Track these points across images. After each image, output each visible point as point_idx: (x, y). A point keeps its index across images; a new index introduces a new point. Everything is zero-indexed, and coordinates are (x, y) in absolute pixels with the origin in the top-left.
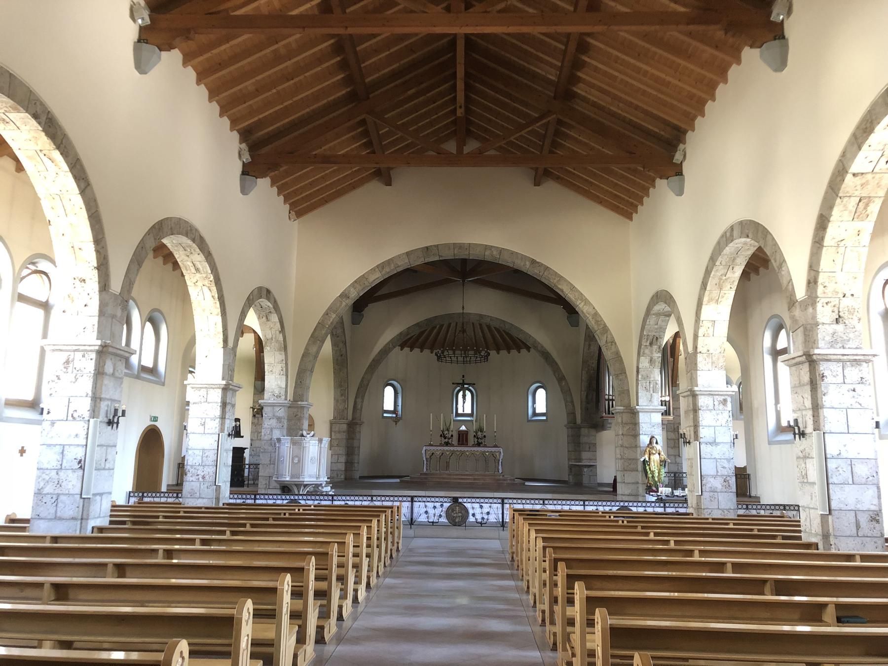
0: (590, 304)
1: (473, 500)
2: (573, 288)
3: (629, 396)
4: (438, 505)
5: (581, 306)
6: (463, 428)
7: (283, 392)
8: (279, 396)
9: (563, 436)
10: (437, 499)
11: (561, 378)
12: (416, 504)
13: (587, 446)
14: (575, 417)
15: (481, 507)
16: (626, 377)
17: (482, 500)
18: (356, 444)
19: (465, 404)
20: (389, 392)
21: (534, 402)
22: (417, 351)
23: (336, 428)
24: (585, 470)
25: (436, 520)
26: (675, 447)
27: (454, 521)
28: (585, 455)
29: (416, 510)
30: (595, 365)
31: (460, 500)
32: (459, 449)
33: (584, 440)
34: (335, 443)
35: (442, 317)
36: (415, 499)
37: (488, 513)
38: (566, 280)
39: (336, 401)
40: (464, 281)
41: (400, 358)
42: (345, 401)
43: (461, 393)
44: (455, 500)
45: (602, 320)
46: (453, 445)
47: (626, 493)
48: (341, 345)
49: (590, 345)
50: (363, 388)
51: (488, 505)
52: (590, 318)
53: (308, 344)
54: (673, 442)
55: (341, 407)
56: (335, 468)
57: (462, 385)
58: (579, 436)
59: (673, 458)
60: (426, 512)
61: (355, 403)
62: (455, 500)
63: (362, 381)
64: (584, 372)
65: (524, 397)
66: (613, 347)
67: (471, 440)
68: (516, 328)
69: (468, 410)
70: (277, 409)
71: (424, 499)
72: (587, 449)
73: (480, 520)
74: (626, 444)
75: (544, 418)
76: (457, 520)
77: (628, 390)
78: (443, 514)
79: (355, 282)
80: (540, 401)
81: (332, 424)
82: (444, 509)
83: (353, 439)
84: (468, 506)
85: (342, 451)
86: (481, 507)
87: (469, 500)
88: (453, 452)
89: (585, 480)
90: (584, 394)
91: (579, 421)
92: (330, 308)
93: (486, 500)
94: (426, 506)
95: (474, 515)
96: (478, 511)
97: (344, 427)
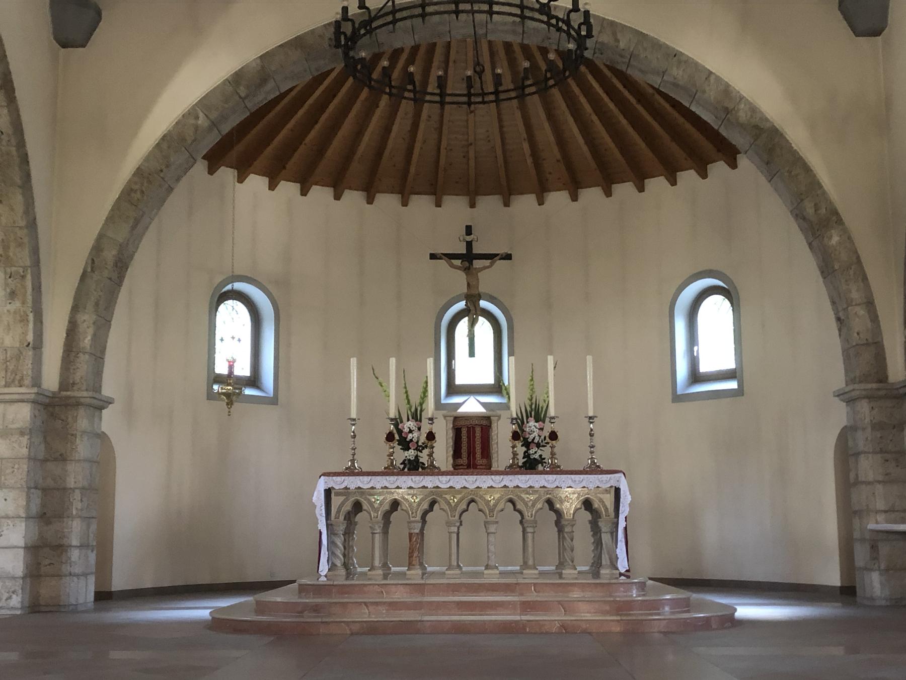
20: (232, 320)
22: (320, 194)
32: (460, 481)
41: (261, 210)
42: (24, 320)
43: (463, 325)
46: (432, 470)
50: (106, 274)
63: (97, 248)
67: (504, 448)
68: (657, 45)
75: (733, 385)
80: (715, 336)
83: (63, 459)
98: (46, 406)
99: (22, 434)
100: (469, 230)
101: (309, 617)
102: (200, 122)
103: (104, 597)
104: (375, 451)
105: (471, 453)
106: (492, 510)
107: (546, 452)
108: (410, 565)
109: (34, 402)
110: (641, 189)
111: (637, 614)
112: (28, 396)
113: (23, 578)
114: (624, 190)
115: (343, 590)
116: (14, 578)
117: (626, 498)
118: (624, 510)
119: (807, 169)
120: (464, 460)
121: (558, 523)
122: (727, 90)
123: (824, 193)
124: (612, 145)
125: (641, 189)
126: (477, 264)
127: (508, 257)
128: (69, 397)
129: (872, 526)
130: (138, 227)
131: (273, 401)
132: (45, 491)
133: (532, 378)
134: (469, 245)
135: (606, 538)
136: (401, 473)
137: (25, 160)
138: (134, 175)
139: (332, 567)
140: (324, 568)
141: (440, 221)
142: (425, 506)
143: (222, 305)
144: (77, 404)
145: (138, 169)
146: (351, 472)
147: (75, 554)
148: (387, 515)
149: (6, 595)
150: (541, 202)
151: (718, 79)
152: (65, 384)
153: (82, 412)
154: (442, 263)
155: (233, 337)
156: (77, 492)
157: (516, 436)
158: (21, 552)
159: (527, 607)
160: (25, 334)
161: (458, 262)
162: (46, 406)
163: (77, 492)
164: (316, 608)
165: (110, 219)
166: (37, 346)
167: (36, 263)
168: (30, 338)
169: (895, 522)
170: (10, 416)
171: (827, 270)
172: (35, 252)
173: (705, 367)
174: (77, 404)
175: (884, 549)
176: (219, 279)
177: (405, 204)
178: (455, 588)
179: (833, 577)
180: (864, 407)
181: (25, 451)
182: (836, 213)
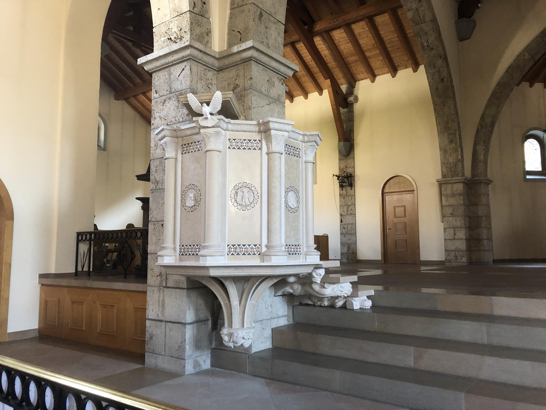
23: (448, 189)
34: (449, 211)
39: (444, 151)
42: (456, 151)
48: (439, 63)
56: (453, 248)
81: (441, 184)
83: (476, 205)
85: (459, 222)
97: (460, 187)
99: (460, 195)
102: (526, 57)
103: (494, 261)
109: (464, 183)
112: (461, 180)
113: (466, 251)
116: (462, 251)
128: (477, 180)
132: (470, 218)
138: (496, 86)
143: (526, 142)
144: (479, 182)
145: (498, 83)
149: (460, 258)
152: (473, 176)
153: (483, 186)
155: (532, 156)
156: (484, 217)
158: (464, 241)
160: (457, 156)
163: (484, 217)
165: (487, 107)
166: (462, 161)
167: (459, 127)
168: (460, 157)
172: (459, 123)
174: (479, 182)
176: (525, 130)
181: (462, 202)
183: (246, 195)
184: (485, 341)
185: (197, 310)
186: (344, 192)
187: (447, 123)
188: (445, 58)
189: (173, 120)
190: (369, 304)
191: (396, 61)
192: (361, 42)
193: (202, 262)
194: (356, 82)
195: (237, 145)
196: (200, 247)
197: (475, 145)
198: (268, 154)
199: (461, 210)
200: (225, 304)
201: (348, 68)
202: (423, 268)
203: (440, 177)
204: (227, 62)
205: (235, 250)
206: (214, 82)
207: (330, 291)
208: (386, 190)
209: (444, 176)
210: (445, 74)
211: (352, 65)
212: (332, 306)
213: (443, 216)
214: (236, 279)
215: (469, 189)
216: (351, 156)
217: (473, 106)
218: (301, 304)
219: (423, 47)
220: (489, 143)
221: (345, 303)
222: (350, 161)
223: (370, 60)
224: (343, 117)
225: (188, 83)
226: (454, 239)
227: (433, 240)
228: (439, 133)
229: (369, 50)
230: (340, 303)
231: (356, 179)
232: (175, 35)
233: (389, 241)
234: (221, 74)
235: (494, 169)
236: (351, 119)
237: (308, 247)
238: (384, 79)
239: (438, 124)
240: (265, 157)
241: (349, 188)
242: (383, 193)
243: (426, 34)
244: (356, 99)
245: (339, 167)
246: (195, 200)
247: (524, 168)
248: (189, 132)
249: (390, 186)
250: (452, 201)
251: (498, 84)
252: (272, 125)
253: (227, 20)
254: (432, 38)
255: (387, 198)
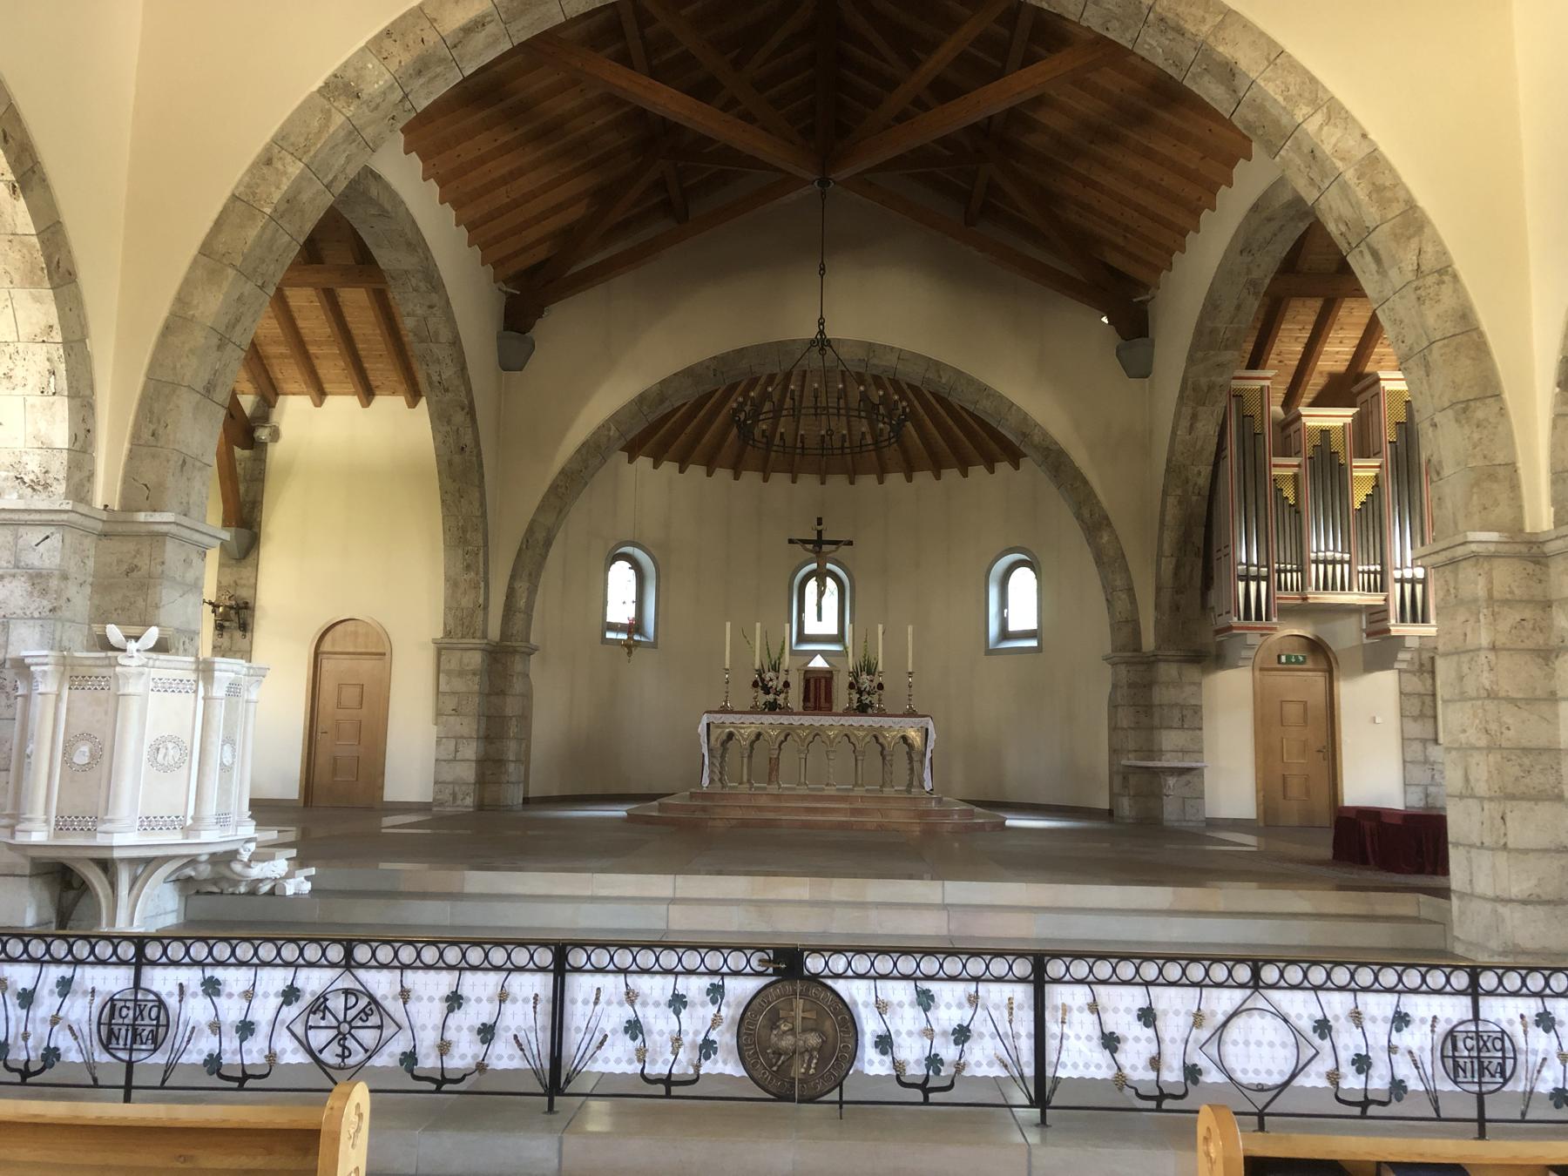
0: (1348, 119)
1: (884, 964)
2: (1276, 55)
3: (1515, 486)
4: (695, 987)
5: (1311, 127)
6: (819, 663)
7: (59, 466)
8: (39, 485)
9: (1094, 689)
10: (691, 959)
11: (1094, 523)
12: (580, 987)
13: (1176, 713)
14: (1136, 633)
15: (925, 1000)
16: (1502, 411)
17: (929, 965)
18: (511, 707)
19: (822, 612)
20: (621, 578)
21: (1003, 603)
22: (696, 471)
23: (452, 661)
24: (1171, 781)
25: (683, 1068)
26: (1422, 715)
27: (782, 1072)
28: (1170, 740)
29: (578, 1014)
30: (1203, 481)
31: (814, 964)
32: (807, 720)
33: (1162, 695)
34: (450, 703)
35: (760, 350)
36: (577, 957)
37: (962, 1034)
38: (1247, 26)
39: (452, 583)
40: (824, 182)
41: (649, 485)
42: (476, 587)
43: (812, 586)
44: (787, 962)
45: (1398, 183)
47: (1515, 891)
48: (459, 418)
49: (1194, 417)
50: (534, 550)
51: (961, 990)
52: (1350, 175)
53: (187, 282)
54: (1416, 701)
55: (466, 602)
56: (449, 778)
57: (819, 548)
58: (1148, 685)
59: (1417, 746)
60: (634, 1028)
61: (511, 594)
62: (787, 962)
63: (530, 530)
64: (1171, 501)
65: (978, 586)
66: (1447, 290)
67: (842, 696)
68: (971, 381)
69: (829, 626)
70: (33, 536)
71: (624, 958)
72: (1176, 723)
73: (916, 1070)
74: (1506, 687)
75: (1034, 643)
76: (798, 1070)
77: (1512, 466)
78: (725, 1038)
79: (388, 33)
80: (1023, 602)
81: (441, 649)
82: (730, 1012)
83: (502, 693)
84: (856, 992)
85: (467, 726)
86: (925, 1000)
87: (861, 964)
88: (788, 733)
89: (1171, 812)
90: (1168, 566)
91: (1149, 641)
92: (280, 140)
93: (953, 966)
94: (631, 997)
95: (884, 1043)
96: (906, 1021)
97: (475, 659)
98: (491, 652)
99: (474, 674)
100: (820, 522)
101: (698, 815)
103: (526, 801)
104: (747, 696)
105: (817, 698)
106: (832, 742)
107: (874, 699)
108: (770, 782)
110: (965, 475)
111: (933, 819)
114: (951, 475)
115: (723, 796)
117: (932, 735)
118: (931, 745)
119: (1085, 482)
120: (811, 704)
121: (909, 754)
122: (1025, 417)
123: (1098, 502)
124: (942, 443)
125: (965, 475)
126: (825, 548)
127: (850, 543)
129: (1124, 762)
130: (561, 512)
131: (654, 645)
132: (488, 717)
133: (865, 640)
134: (820, 533)
135: (916, 765)
136: (762, 712)
137: (481, 465)
139: (712, 781)
140: (706, 782)
141: (792, 498)
142: (782, 738)
144: (514, 651)
146: (724, 710)
147: (511, 767)
148: (724, 744)
150: (881, 481)
151: (1019, 409)
152: (504, 635)
154: (798, 547)
155: (621, 593)
157: (851, 686)
159: (855, 812)
160: (477, 597)
161: (810, 547)
162: (491, 652)
164: (704, 809)
166: (486, 608)
168: (481, 601)
169: (1143, 759)
170: (466, 661)
171: (1099, 560)
173: (1013, 627)
174: (514, 651)
175: (1133, 780)
176: (612, 544)
177: (765, 480)
178: (804, 798)
179: (1104, 803)
180: (1123, 669)
182: (1107, 518)
183: (171, 752)
184: (447, 923)
185: (39, 908)
186: (225, 641)
187: (464, 531)
188: (471, 412)
189: (19, 612)
190: (307, 887)
191: (374, 378)
192: (300, 323)
193: (101, 840)
194: (277, 395)
195: (165, 687)
196: (96, 819)
197: (513, 577)
198: (204, 699)
199: (473, 704)
200: (106, 896)
201: (263, 365)
202: (388, 821)
203: (439, 634)
204: (120, 528)
205: (148, 823)
206: (92, 552)
207: (257, 871)
208: (326, 646)
209: (448, 634)
210: (467, 439)
211: (274, 361)
212: (252, 892)
213: (439, 713)
214: (132, 861)
215: (492, 666)
216: (250, 559)
217: (516, 505)
218: (198, 892)
219: (430, 383)
220: (538, 575)
221: (273, 888)
222: (246, 572)
223: (316, 362)
224: (239, 470)
225: (58, 561)
226: (455, 760)
227: (416, 754)
228: (448, 547)
229: (319, 344)
230: (265, 888)
231: (258, 614)
232: (32, 476)
233: (322, 760)
234: (105, 542)
235: (549, 617)
236: (258, 476)
237: (240, 814)
238: (343, 405)
239: (447, 530)
240: (201, 703)
241: (238, 634)
242: (317, 654)
243: (438, 361)
244: (275, 435)
245: (219, 582)
246: (92, 756)
247: (604, 614)
248: (88, 662)
249: (334, 640)
250: (459, 685)
251: (563, 472)
252: (217, 666)
253: (123, 459)
254: (449, 372)
255: (327, 665)
